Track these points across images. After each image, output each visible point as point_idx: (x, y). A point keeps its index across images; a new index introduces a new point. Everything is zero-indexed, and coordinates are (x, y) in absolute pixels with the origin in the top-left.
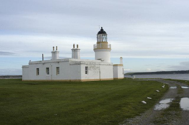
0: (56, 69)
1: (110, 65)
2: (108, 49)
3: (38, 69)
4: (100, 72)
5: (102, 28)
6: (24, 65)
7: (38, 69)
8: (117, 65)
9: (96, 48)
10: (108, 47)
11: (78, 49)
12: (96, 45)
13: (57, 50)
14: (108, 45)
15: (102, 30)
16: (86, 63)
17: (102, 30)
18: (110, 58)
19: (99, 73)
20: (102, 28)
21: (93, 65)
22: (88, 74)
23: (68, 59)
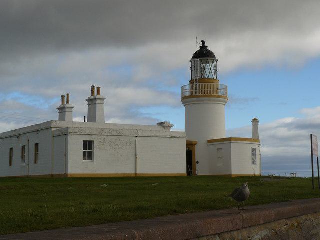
0: (34, 146)
1: (174, 137)
2: (221, 97)
3: (11, 149)
4: (136, 155)
5: (203, 42)
6: (39, 145)
7: (11, 149)
8: (229, 139)
9: (188, 94)
10: (221, 93)
11: (98, 97)
12: (188, 88)
13: (68, 103)
14: (221, 87)
15: (204, 47)
16: (87, 132)
17: (204, 47)
18: (231, 121)
19: (133, 159)
20: (203, 42)
21: (110, 138)
22: (93, 162)
23: (50, 122)
